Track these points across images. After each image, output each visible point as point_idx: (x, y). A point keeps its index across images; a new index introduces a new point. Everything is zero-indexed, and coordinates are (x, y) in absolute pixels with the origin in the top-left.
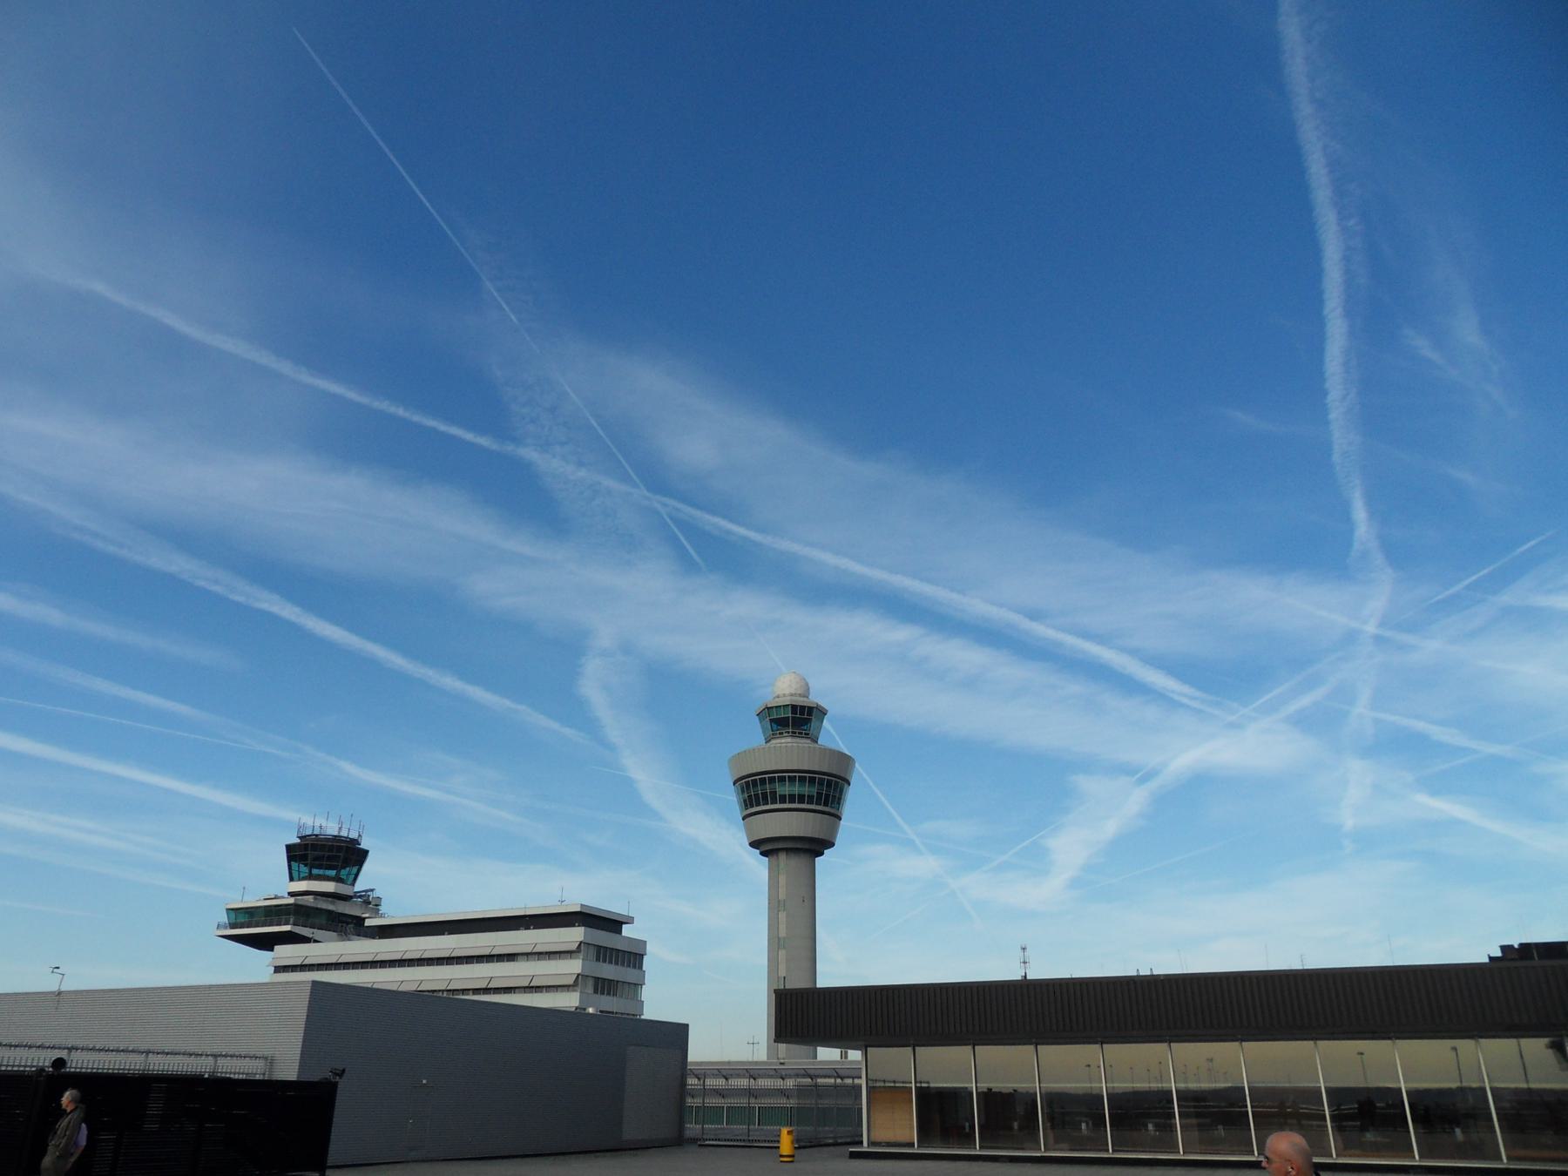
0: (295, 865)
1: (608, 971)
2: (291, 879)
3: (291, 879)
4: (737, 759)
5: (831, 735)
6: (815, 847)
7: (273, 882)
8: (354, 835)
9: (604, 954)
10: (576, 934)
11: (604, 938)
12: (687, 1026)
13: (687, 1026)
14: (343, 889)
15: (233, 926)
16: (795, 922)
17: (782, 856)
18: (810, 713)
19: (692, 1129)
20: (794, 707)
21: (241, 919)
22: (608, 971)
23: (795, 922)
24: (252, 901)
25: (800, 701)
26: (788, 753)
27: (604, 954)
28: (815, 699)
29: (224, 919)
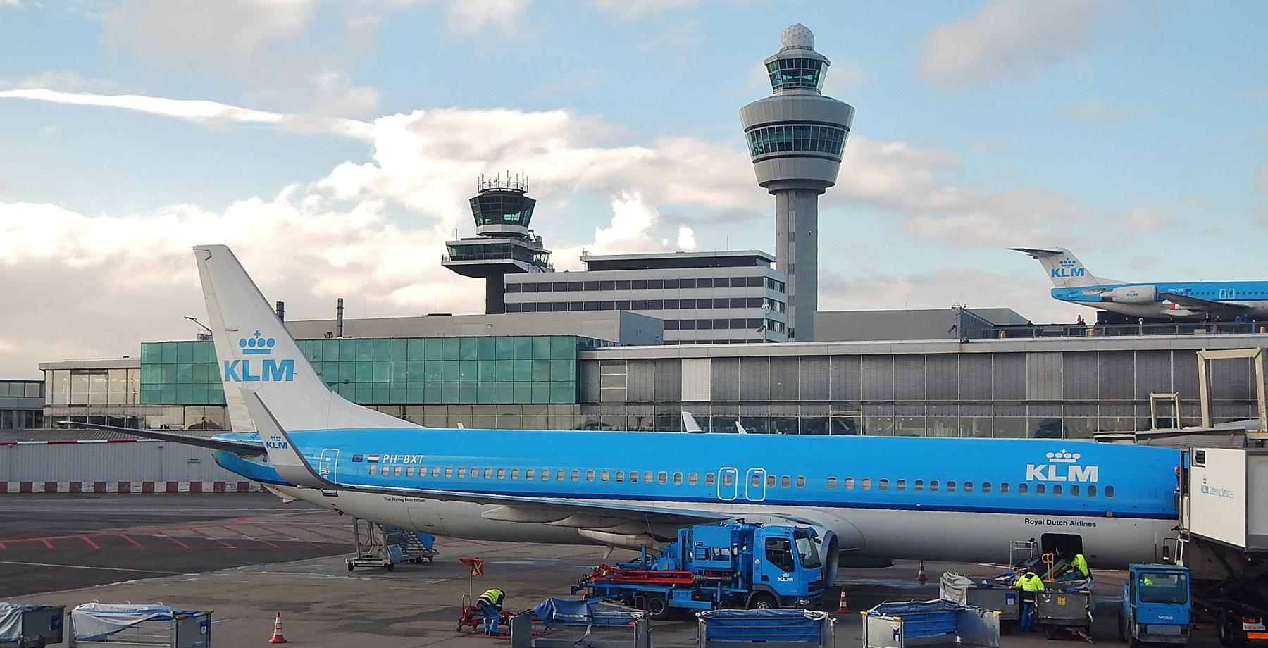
4: (750, 109)
5: (831, 85)
7: (468, 228)
15: (453, 258)
28: (819, 49)
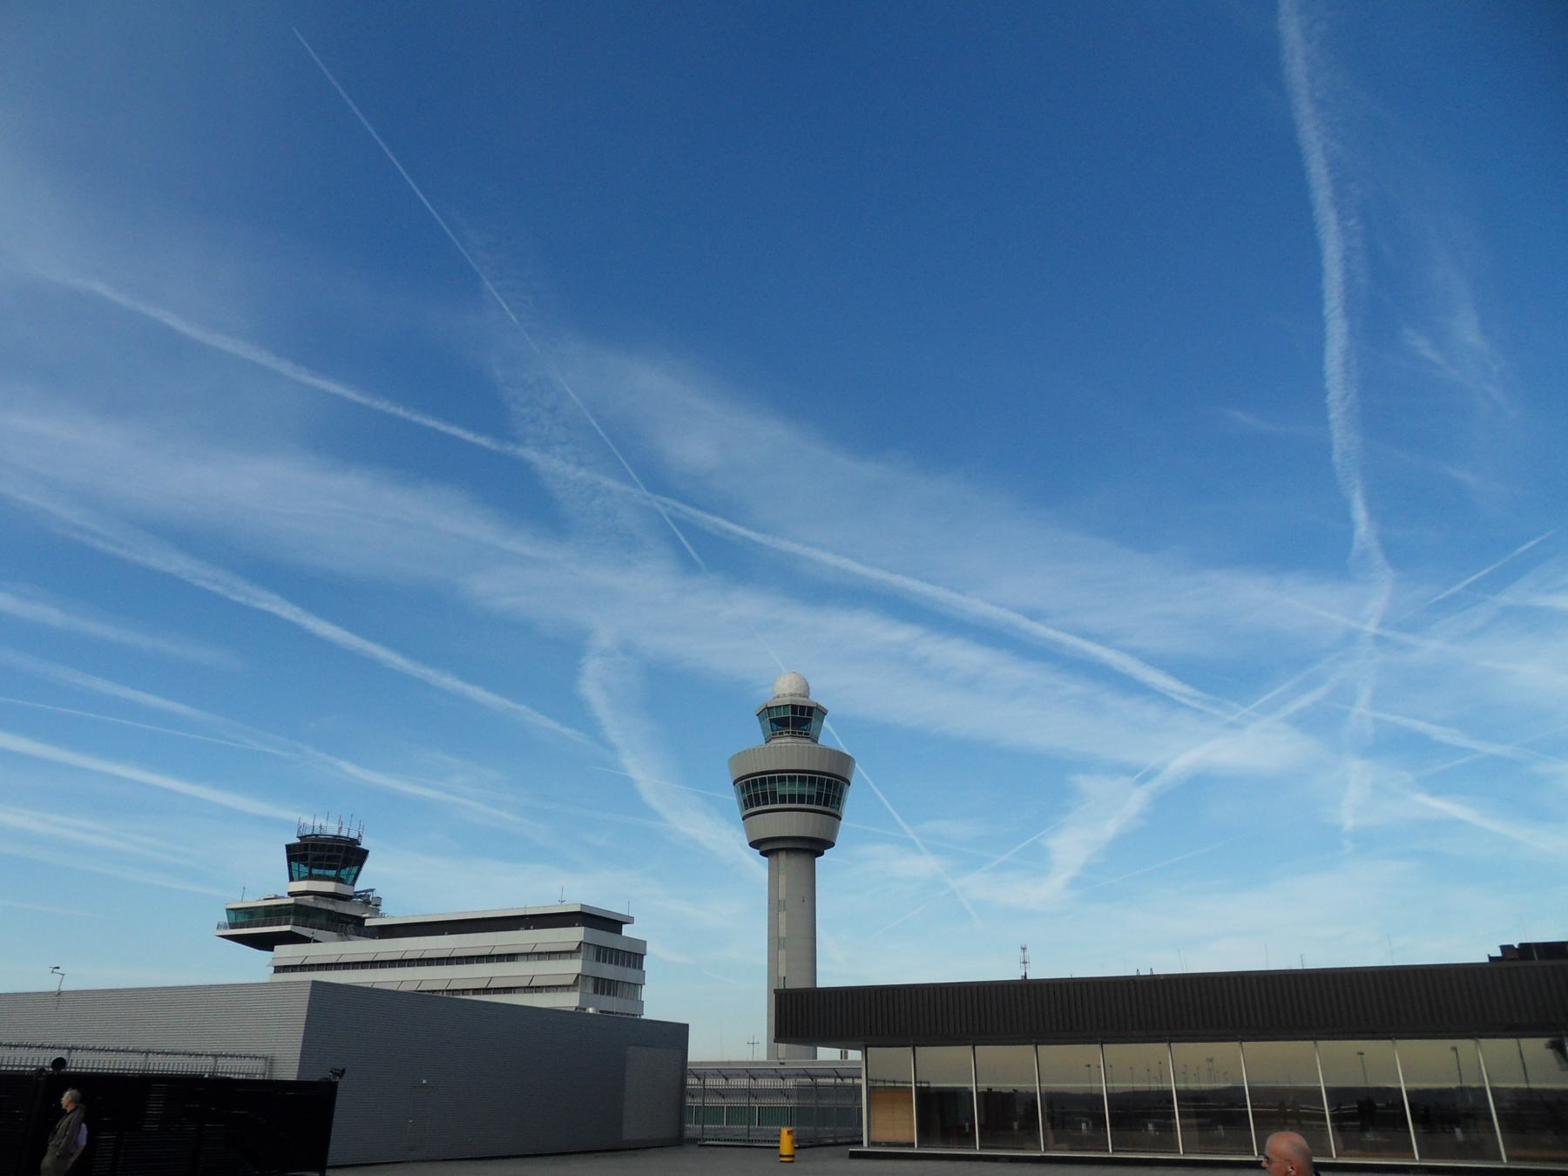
0: (295, 865)
1: (608, 971)
2: (291, 879)
3: (291, 879)
4: (737, 759)
5: (831, 735)
6: (815, 847)
7: (273, 882)
8: (354, 835)
9: (604, 954)
10: (576, 934)
11: (604, 938)
12: (687, 1026)
13: (687, 1026)
14: (343, 889)
15: (233, 926)
16: (795, 922)
17: (782, 856)
18: (810, 713)
19: (692, 1129)
20: (794, 707)
21: (241, 919)
22: (608, 971)
23: (795, 922)
24: (252, 901)
25: (800, 701)
26: (788, 753)
27: (604, 954)
28: (815, 699)
29: (224, 919)
